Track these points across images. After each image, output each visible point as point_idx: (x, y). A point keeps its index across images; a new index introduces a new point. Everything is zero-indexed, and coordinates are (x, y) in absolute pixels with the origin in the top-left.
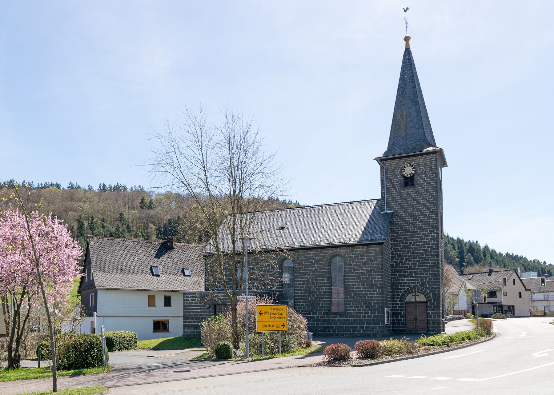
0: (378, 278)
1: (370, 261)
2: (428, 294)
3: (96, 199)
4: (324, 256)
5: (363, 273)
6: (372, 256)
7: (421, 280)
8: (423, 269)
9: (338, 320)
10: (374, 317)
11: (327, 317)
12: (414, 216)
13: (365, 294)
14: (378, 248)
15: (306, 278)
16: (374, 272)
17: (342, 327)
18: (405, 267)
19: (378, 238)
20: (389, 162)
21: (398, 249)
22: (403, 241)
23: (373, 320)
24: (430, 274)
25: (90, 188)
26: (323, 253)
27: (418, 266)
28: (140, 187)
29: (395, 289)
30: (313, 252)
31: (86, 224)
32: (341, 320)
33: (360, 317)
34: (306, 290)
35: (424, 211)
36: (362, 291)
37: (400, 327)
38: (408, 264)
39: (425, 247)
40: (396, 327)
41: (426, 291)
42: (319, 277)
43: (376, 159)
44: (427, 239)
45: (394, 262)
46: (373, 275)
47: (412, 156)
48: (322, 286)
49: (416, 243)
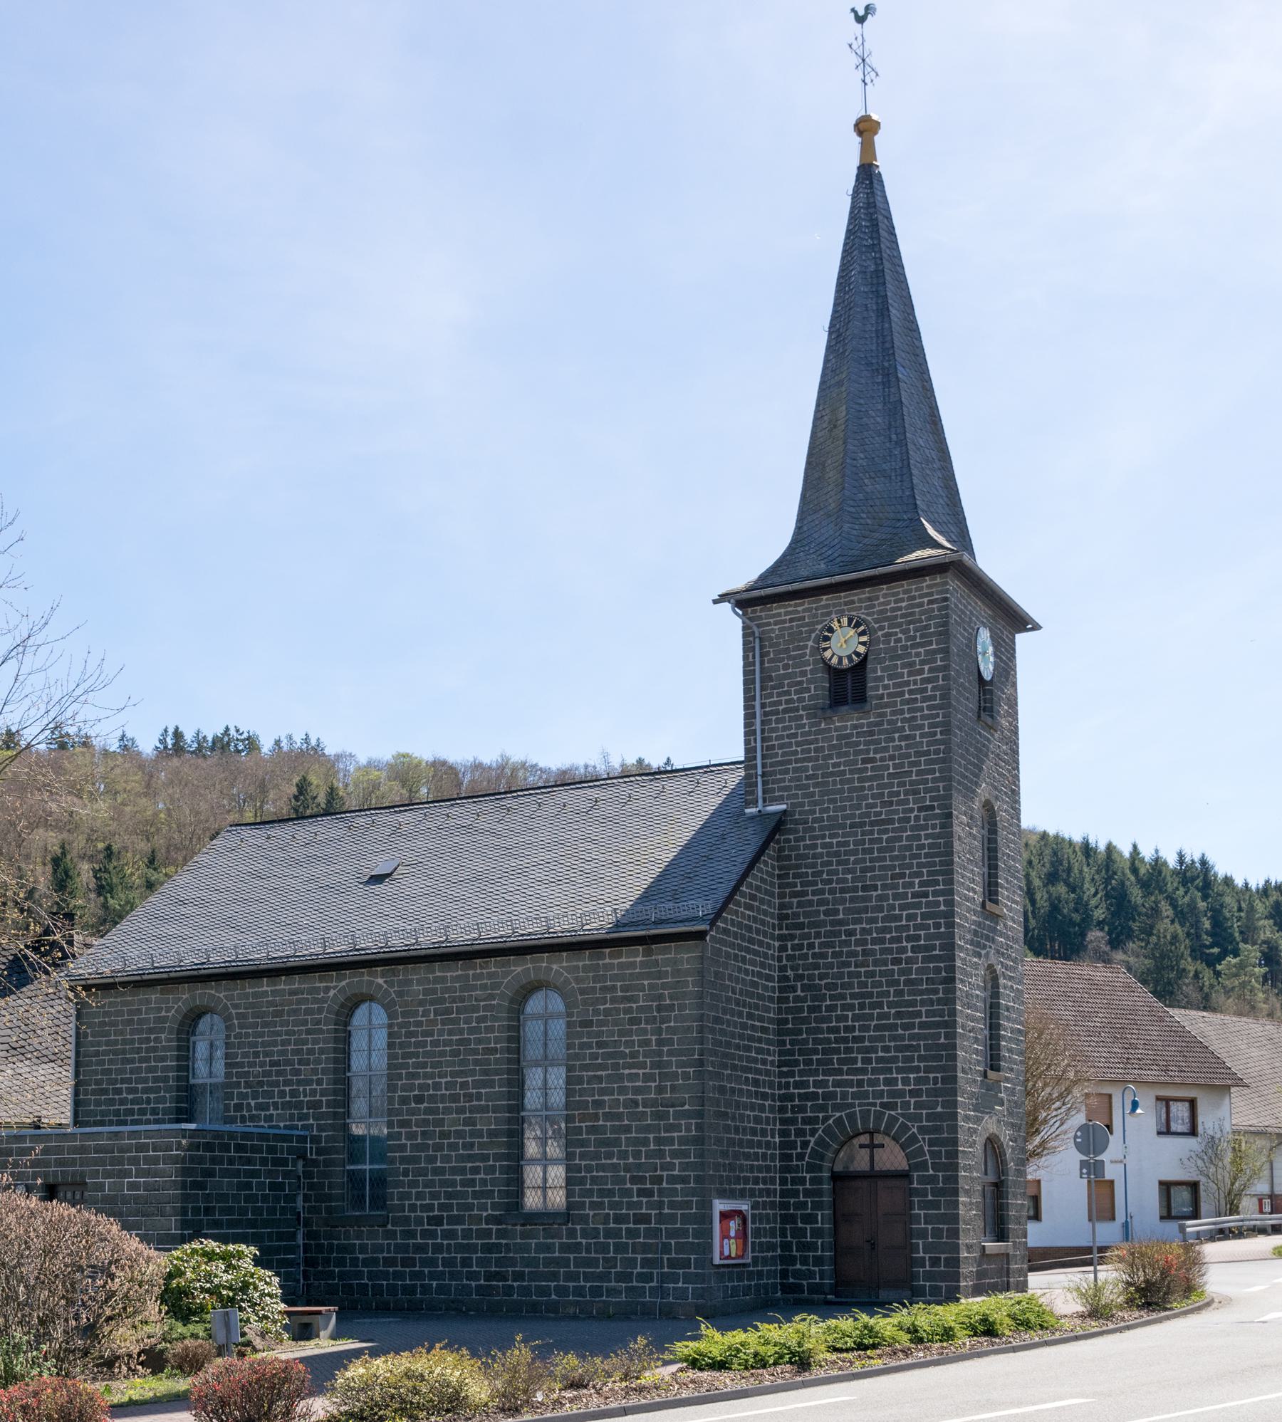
0: (686, 1076)
1: (659, 1009)
2: (913, 1139)
3: (135, 781)
4: (496, 986)
5: (634, 1055)
6: (664, 986)
7: (888, 1082)
8: (893, 1038)
9: (540, 1248)
10: (671, 1234)
11: (501, 1234)
12: (862, 824)
13: (637, 1142)
14: (685, 956)
15: (426, 1076)
16: (670, 1053)
17: (554, 1276)
18: (830, 1030)
19: (684, 915)
20: (778, 610)
21: (805, 957)
22: (823, 924)
23: (666, 1248)
24: (921, 1059)
25: (127, 746)
26: (490, 976)
27: (877, 1028)
28: (307, 740)
29: (793, 1121)
30: (454, 972)
31: (85, 873)
32: (549, 1248)
33: (616, 1234)
34: (425, 1122)
35: (900, 803)
36: (627, 1129)
37: (811, 1274)
38: (839, 1019)
39: (904, 950)
40: (797, 1274)
41: (904, 1128)
42: (473, 1073)
43: (1036, 627)
44: (909, 918)
45: (788, 1011)
46: (669, 1063)
47: (878, 590)
48: (484, 1109)
49: (869, 932)
